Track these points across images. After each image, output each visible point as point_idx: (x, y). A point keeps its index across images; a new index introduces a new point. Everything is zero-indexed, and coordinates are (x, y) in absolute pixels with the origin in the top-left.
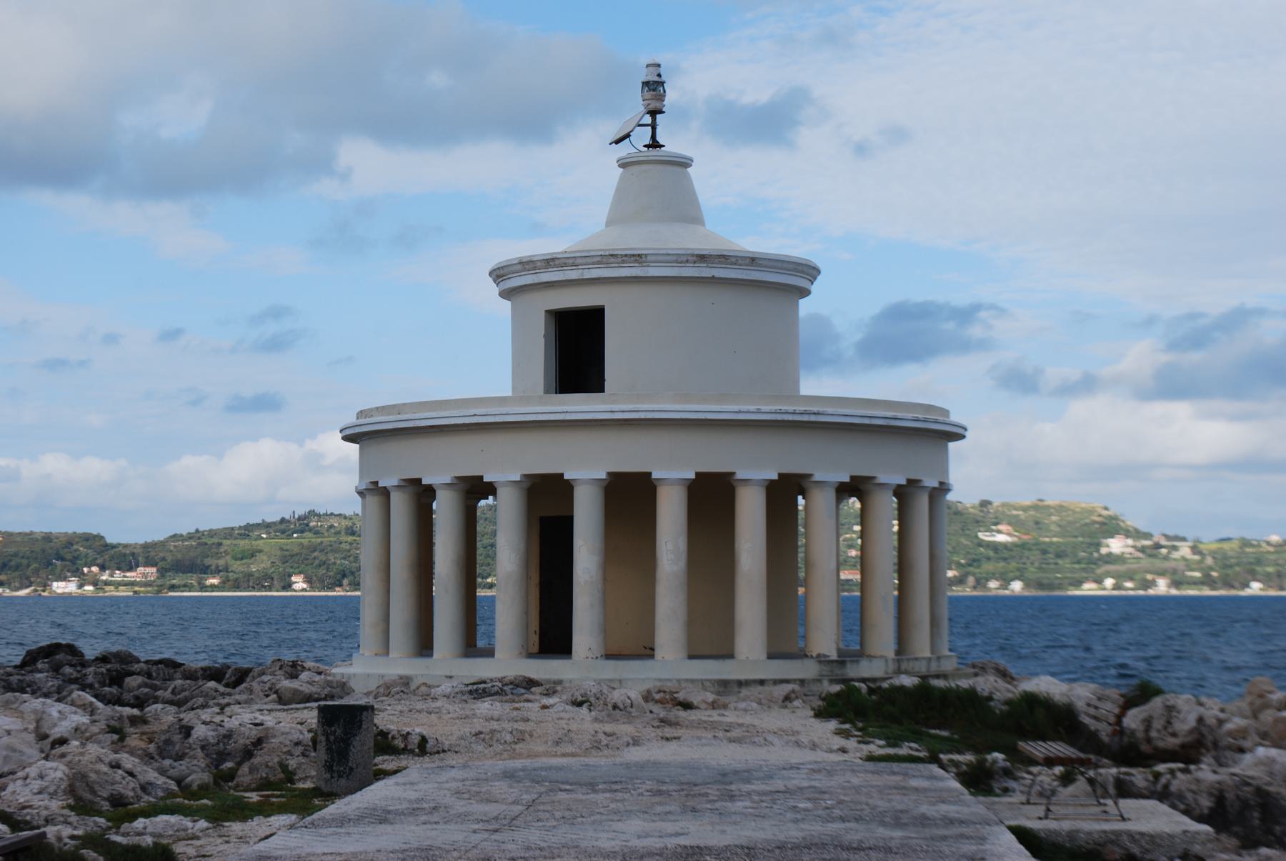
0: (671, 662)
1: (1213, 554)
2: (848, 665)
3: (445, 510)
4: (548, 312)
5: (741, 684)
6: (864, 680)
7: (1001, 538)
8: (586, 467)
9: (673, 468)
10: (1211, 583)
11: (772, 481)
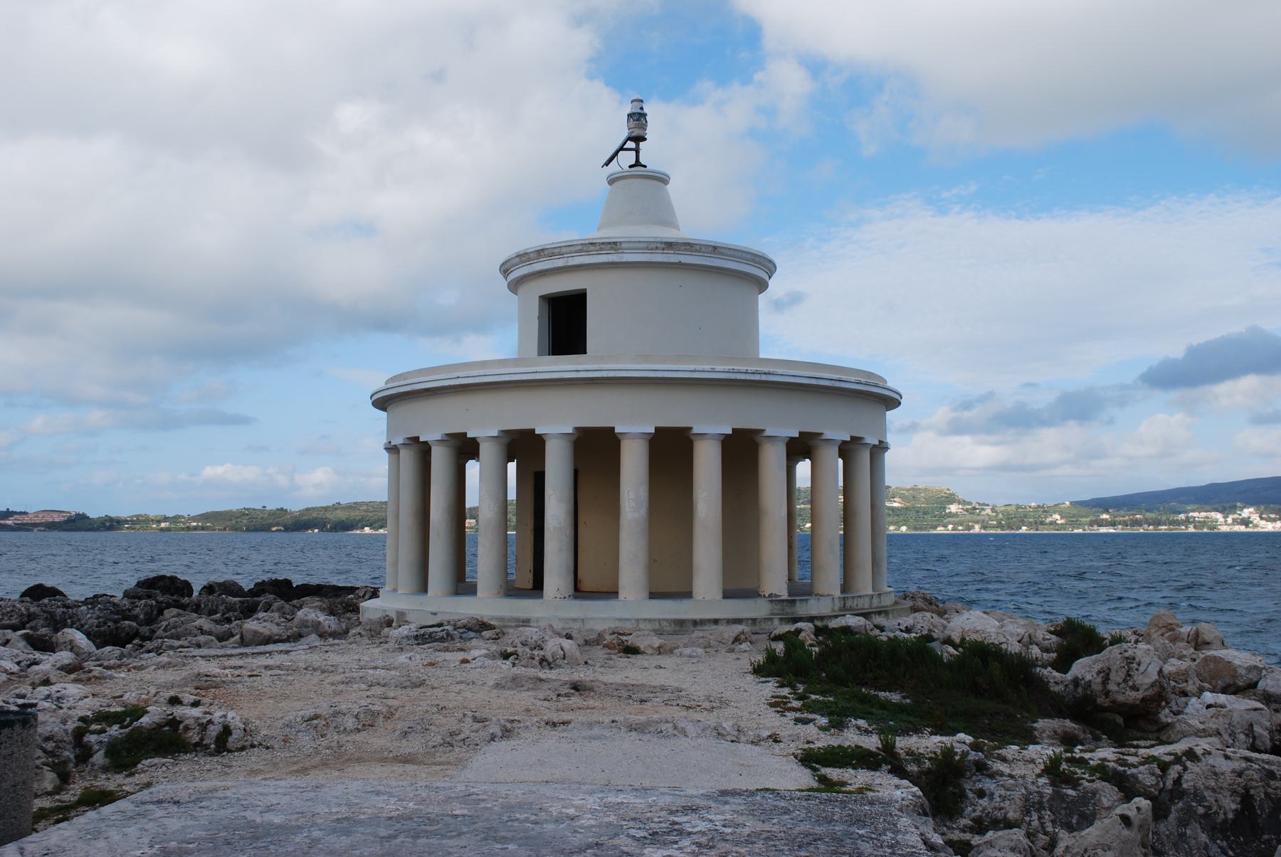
0: (632, 605)
1: (1003, 512)
2: (798, 603)
3: (440, 461)
4: (542, 298)
5: (695, 623)
6: (811, 619)
7: (895, 505)
8: (556, 422)
9: (634, 422)
10: (1002, 527)
11: (727, 436)
